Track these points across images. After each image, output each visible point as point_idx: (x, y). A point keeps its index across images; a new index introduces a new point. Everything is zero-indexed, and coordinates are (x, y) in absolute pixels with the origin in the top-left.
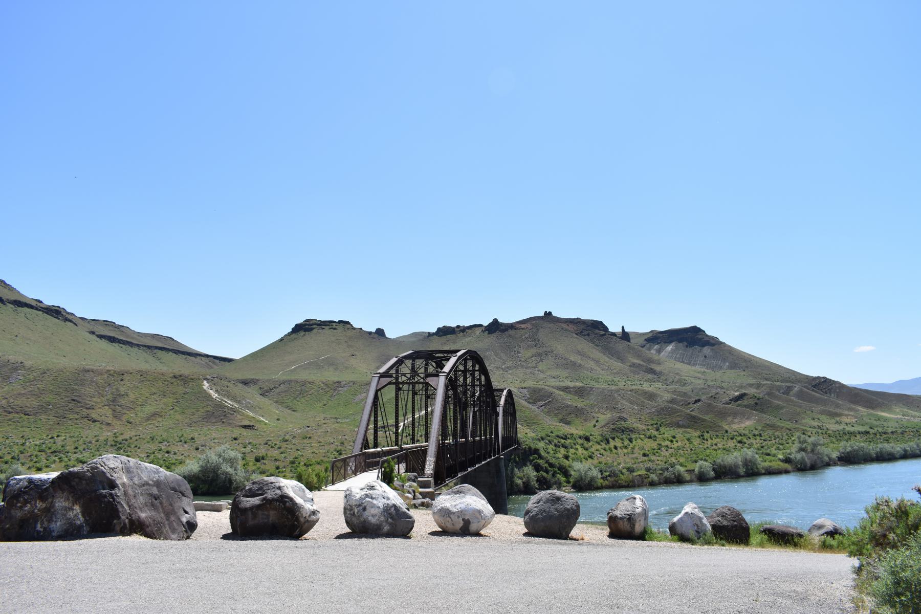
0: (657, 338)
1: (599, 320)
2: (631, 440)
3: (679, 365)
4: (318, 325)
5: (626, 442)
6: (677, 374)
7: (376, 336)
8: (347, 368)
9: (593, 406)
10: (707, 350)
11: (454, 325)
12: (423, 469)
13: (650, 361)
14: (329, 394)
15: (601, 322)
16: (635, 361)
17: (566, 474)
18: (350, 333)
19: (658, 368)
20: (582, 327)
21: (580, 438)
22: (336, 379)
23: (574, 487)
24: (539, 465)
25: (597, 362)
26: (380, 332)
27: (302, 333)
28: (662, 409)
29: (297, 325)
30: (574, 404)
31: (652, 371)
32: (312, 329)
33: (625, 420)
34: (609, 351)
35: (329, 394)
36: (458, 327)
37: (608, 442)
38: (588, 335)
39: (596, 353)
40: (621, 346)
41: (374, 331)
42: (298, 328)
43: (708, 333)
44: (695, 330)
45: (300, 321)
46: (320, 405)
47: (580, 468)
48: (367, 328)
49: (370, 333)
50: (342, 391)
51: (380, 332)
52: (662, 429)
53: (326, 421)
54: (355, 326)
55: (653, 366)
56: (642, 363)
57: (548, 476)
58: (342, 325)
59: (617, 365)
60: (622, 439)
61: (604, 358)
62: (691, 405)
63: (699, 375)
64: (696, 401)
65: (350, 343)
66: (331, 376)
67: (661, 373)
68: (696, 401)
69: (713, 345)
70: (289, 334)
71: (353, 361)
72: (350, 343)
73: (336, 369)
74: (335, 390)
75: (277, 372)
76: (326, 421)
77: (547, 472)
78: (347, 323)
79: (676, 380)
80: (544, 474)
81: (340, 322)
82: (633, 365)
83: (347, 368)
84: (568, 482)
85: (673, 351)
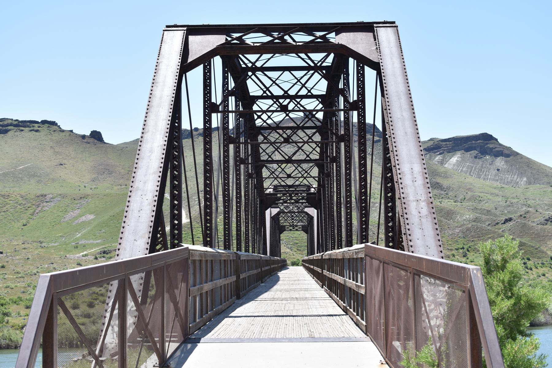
3: (471, 180)
4: (16, 126)
6: (469, 189)
7: (92, 140)
8: (53, 180)
10: (500, 162)
12: (251, 146)
14: (31, 211)
18: (57, 136)
19: (445, 183)
22: (39, 193)
26: (96, 136)
28: (468, 229)
32: (6, 132)
35: (31, 211)
41: (88, 133)
43: (500, 141)
44: (487, 138)
48: (79, 131)
49: (84, 137)
50: (48, 207)
51: (96, 136)
53: (26, 246)
54: (63, 127)
55: (439, 180)
58: (47, 125)
62: (500, 226)
63: (496, 191)
64: (506, 221)
65: (57, 149)
66: (31, 188)
67: (448, 188)
68: (506, 221)
69: (508, 156)
71: (61, 173)
72: (57, 149)
73: (39, 182)
74: (38, 206)
75: (382, 342)
76: (26, 246)
78: (53, 123)
79: (467, 198)
81: (44, 122)
83: (53, 180)
85: (458, 163)
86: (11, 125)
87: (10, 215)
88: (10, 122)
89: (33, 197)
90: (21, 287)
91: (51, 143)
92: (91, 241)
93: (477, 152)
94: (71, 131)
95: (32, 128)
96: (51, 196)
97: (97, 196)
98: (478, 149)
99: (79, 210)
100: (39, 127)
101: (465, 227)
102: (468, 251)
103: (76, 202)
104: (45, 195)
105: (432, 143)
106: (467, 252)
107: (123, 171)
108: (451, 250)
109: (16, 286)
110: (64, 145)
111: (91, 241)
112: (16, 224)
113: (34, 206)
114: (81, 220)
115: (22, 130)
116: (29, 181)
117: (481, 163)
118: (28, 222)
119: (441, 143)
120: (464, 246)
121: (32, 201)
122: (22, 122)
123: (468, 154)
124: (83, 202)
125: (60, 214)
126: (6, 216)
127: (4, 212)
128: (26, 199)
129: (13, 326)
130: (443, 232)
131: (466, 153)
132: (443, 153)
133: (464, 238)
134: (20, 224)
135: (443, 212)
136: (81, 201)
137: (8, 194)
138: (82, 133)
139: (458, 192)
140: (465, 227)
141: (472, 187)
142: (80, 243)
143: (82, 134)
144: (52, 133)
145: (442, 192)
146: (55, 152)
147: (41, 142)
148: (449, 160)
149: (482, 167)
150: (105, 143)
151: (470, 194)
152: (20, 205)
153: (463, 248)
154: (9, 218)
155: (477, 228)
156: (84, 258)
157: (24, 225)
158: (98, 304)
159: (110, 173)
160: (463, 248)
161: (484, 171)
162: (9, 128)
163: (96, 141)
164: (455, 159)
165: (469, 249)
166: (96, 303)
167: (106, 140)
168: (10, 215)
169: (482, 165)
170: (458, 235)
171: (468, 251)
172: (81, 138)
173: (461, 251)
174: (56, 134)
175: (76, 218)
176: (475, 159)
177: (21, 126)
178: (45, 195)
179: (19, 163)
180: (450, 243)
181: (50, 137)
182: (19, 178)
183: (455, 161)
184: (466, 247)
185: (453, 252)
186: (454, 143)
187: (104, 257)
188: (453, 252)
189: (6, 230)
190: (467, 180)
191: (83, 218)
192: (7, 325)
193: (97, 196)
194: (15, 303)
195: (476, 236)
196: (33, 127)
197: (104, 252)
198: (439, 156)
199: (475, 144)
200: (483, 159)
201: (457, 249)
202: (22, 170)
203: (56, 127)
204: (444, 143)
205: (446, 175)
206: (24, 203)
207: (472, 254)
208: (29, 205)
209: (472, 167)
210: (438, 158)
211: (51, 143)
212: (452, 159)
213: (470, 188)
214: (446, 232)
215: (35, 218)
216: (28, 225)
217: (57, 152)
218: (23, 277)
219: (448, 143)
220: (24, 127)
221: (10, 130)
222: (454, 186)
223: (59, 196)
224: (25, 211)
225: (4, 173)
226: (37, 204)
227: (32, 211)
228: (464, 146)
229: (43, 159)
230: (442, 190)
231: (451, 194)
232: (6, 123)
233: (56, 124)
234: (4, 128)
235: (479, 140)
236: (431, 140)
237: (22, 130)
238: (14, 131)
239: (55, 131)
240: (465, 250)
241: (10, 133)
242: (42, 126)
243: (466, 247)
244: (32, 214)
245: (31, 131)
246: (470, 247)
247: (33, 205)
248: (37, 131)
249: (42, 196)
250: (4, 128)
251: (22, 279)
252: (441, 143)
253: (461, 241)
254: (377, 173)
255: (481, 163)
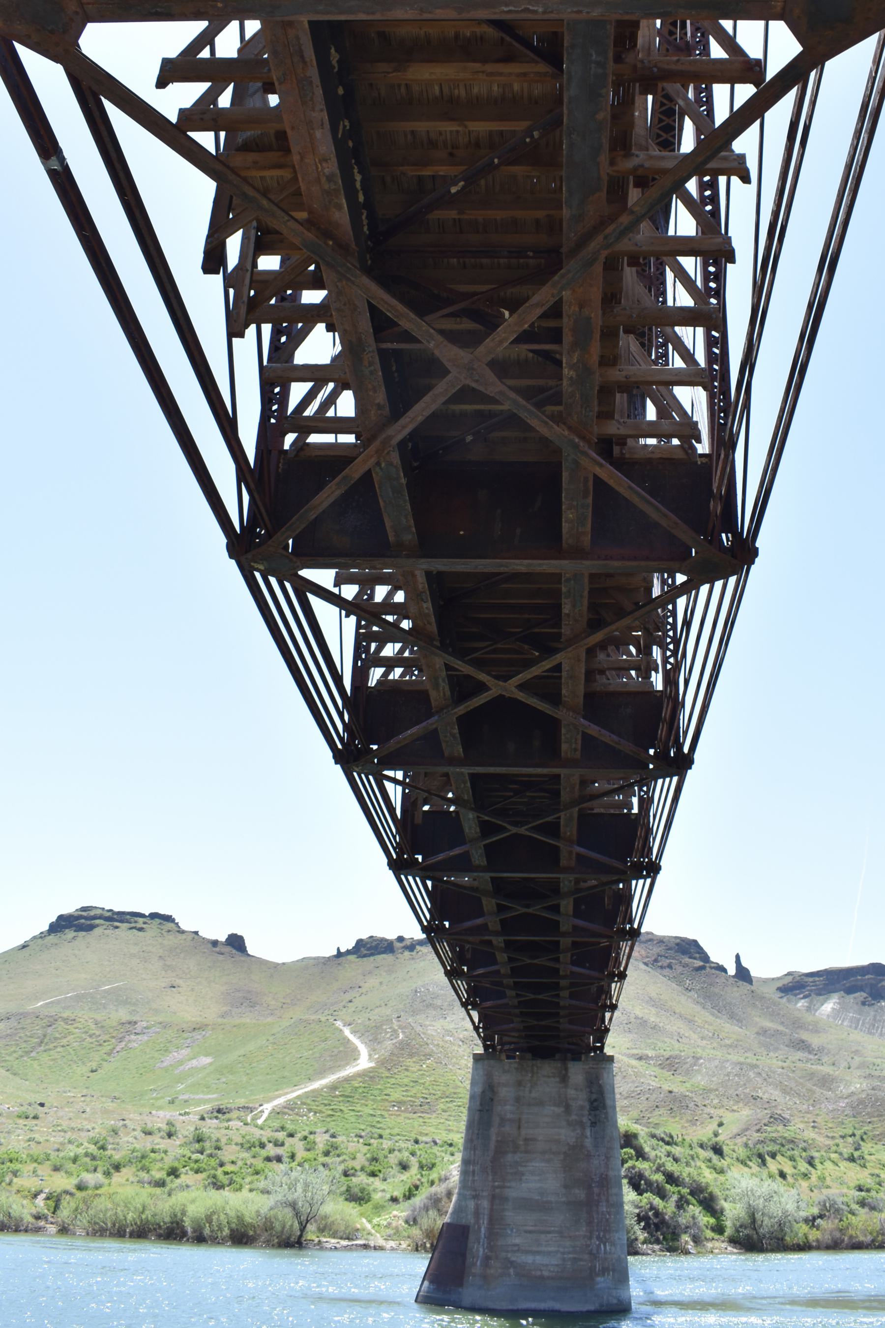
0: (796, 986)
1: (691, 937)
2: (811, 1162)
3: (857, 1036)
5: (803, 1166)
6: (856, 1052)
7: (228, 949)
9: (707, 1091)
11: (391, 936)
13: (797, 1024)
14: (107, 1048)
15: (695, 942)
16: (768, 1024)
17: (709, 1204)
18: (172, 940)
19: (815, 1041)
20: (656, 950)
21: (701, 1146)
23: (734, 1241)
24: (641, 1176)
25: (690, 1021)
26: (236, 942)
27: (70, 934)
28: (861, 1102)
29: (61, 917)
30: (666, 1087)
31: (802, 1045)
32: (91, 928)
33: (785, 1122)
34: (711, 999)
35: (107, 1048)
36: (401, 939)
37: (764, 1163)
38: (670, 966)
39: (686, 1004)
40: (737, 993)
41: (223, 938)
42: (64, 924)
45: (69, 909)
46: (83, 1069)
47: (742, 1188)
49: (215, 943)
50: (136, 1042)
51: (236, 942)
52: (866, 1147)
54: (183, 927)
55: (805, 1036)
56: (781, 1028)
57: (668, 1208)
58: (158, 921)
59: (730, 1029)
60: (792, 1159)
61: (703, 1015)
67: (821, 1050)
70: (42, 936)
74: (121, 1040)
77: (662, 1194)
78: (168, 919)
80: (657, 1201)
81: (154, 916)
82: (763, 1032)
84: (719, 1229)
85: (836, 1014)
86: (101, 917)
87: (72, 1052)
88: (99, 912)
89: (115, 1024)
90: (54, 1142)
91: (161, 951)
92: (201, 1096)
93: (865, 995)
94: (196, 933)
95: (133, 925)
96: (144, 1024)
97: (222, 1027)
98: (868, 990)
99: (189, 1050)
100: (145, 923)
101: (856, 1097)
102: (862, 1139)
103: (185, 1035)
104: (136, 1023)
105: (790, 978)
106: (861, 1143)
107: (273, 1002)
108: (833, 1138)
109: (47, 1141)
110: (182, 955)
111: (201, 1096)
112: (79, 1069)
113: (113, 1040)
114: (190, 1066)
115: (117, 927)
116: (117, 1011)
117: (872, 1013)
118: (100, 1066)
119: (806, 979)
120: (856, 1132)
121: (111, 1030)
122: (119, 913)
123: (850, 999)
124: (197, 1035)
125: (156, 1055)
126: (64, 1054)
127: (63, 1046)
128: (102, 1027)
129: (18, 1191)
130: (818, 1106)
131: (848, 997)
132: (809, 995)
133: (854, 1117)
134: (85, 1070)
135: (816, 1079)
136: (194, 1034)
137: (73, 1018)
138: (212, 937)
139: (837, 1057)
140: (856, 1097)
141: (860, 1048)
142: (180, 1098)
143: (214, 938)
144: (165, 934)
145: (811, 1057)
146: (165, 965)
147: (145, 948)
148: (819, 1008)
149: (875, 1019)
150: (249, 955)
151: (857, 1060)
152: (91, 1036)
153: (854, 1135)
154: (70, 1057)
155: (877, 1100)
156: (181, 1117)
157: (92, 1071)
158: (186, 1174)
159: (253, 1005)
160: (854, 1135)
161: (878, 1027)
162: (97, 922)
163: (234, 951)
164: (829, 1006)
165: (865, 1137)
166: (184, 1170)
167: (251, 950)
168: (72, 1052)
169: (875, 1016)
170: (843, 1111)
171: (862, 1139)
172: (210, 946)
173: (850, 1140)
174: (171, 937)
175: (181, 1062)
176: (863, 1007)
177: (117, 921)
178: (136, 1023)
179: (104, 980)
180: (830, 1125)
181: (160, 940)
182: (101, 1004)
183: (829, 1009)
184: (858, 1133)
185: (837, 1141)
186: (827, 979)
187: (216, 1118)
188: (837, 1141)
189: (61, 1078)
190: (852, 1037)
191: (194, 1063)
192: (8, 1187)
193: (222, 1027)
194: (36, 1161)
195: (876, 1114)
196: (136, 922)
197: (219, 1111)
198: (803, 1001)
199: (861, 980)
200: (876, 1007)
201: (843, 1137)
202: (107, 992)
203: (172, 925)
204: (811, 979)
205: (816, 1029)
206: (98, 1033)
207: (870, 1145)
208: (106, 1037)
209: (859, 1020)
210: (802, 1004)
211: (161, 951)
212: (825, 1005)
213: (857, 1051)
214: (823, 1106)
215: (112, 1060)
216: (100, 1071)
217: (169, 966)
218: (65, 1132)
219: (817, 979)
220: (122, 921)
221: (97, 926)
222: (830, 1046)
223: (158, 1025)
224: (99, 1048)
225: (77, 996)
226: (120, 1036)
227: (109, 1048)
228: (844, 985)
229: (144, 976)
230: (810, 1052)
231: (825, 1059)
232: (92, 913)
233: (173, 921)
234: (89, 922)
235: (868, 973)
236: (789, 974)
237: (117, 927)
238: (105, 927)
239: (169, 931)
240: (858, 1137)
241: (97, 931)
242: (149, 922)
243: (858, 1133)
244: (109, 1054)
245: (131, 928)
246: (865, 1133)
247: (113, 1037)
248: (141, 929)
249: (130, 1023)
250: (89, 922)
251: (62, 1134)
252: (806, 979)
253: (850, 1122)
254: (700, 1021)
255: (872, 1013)
